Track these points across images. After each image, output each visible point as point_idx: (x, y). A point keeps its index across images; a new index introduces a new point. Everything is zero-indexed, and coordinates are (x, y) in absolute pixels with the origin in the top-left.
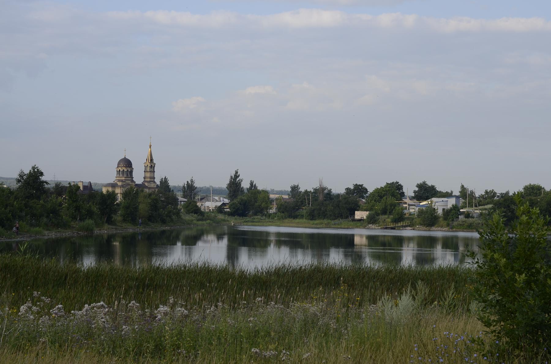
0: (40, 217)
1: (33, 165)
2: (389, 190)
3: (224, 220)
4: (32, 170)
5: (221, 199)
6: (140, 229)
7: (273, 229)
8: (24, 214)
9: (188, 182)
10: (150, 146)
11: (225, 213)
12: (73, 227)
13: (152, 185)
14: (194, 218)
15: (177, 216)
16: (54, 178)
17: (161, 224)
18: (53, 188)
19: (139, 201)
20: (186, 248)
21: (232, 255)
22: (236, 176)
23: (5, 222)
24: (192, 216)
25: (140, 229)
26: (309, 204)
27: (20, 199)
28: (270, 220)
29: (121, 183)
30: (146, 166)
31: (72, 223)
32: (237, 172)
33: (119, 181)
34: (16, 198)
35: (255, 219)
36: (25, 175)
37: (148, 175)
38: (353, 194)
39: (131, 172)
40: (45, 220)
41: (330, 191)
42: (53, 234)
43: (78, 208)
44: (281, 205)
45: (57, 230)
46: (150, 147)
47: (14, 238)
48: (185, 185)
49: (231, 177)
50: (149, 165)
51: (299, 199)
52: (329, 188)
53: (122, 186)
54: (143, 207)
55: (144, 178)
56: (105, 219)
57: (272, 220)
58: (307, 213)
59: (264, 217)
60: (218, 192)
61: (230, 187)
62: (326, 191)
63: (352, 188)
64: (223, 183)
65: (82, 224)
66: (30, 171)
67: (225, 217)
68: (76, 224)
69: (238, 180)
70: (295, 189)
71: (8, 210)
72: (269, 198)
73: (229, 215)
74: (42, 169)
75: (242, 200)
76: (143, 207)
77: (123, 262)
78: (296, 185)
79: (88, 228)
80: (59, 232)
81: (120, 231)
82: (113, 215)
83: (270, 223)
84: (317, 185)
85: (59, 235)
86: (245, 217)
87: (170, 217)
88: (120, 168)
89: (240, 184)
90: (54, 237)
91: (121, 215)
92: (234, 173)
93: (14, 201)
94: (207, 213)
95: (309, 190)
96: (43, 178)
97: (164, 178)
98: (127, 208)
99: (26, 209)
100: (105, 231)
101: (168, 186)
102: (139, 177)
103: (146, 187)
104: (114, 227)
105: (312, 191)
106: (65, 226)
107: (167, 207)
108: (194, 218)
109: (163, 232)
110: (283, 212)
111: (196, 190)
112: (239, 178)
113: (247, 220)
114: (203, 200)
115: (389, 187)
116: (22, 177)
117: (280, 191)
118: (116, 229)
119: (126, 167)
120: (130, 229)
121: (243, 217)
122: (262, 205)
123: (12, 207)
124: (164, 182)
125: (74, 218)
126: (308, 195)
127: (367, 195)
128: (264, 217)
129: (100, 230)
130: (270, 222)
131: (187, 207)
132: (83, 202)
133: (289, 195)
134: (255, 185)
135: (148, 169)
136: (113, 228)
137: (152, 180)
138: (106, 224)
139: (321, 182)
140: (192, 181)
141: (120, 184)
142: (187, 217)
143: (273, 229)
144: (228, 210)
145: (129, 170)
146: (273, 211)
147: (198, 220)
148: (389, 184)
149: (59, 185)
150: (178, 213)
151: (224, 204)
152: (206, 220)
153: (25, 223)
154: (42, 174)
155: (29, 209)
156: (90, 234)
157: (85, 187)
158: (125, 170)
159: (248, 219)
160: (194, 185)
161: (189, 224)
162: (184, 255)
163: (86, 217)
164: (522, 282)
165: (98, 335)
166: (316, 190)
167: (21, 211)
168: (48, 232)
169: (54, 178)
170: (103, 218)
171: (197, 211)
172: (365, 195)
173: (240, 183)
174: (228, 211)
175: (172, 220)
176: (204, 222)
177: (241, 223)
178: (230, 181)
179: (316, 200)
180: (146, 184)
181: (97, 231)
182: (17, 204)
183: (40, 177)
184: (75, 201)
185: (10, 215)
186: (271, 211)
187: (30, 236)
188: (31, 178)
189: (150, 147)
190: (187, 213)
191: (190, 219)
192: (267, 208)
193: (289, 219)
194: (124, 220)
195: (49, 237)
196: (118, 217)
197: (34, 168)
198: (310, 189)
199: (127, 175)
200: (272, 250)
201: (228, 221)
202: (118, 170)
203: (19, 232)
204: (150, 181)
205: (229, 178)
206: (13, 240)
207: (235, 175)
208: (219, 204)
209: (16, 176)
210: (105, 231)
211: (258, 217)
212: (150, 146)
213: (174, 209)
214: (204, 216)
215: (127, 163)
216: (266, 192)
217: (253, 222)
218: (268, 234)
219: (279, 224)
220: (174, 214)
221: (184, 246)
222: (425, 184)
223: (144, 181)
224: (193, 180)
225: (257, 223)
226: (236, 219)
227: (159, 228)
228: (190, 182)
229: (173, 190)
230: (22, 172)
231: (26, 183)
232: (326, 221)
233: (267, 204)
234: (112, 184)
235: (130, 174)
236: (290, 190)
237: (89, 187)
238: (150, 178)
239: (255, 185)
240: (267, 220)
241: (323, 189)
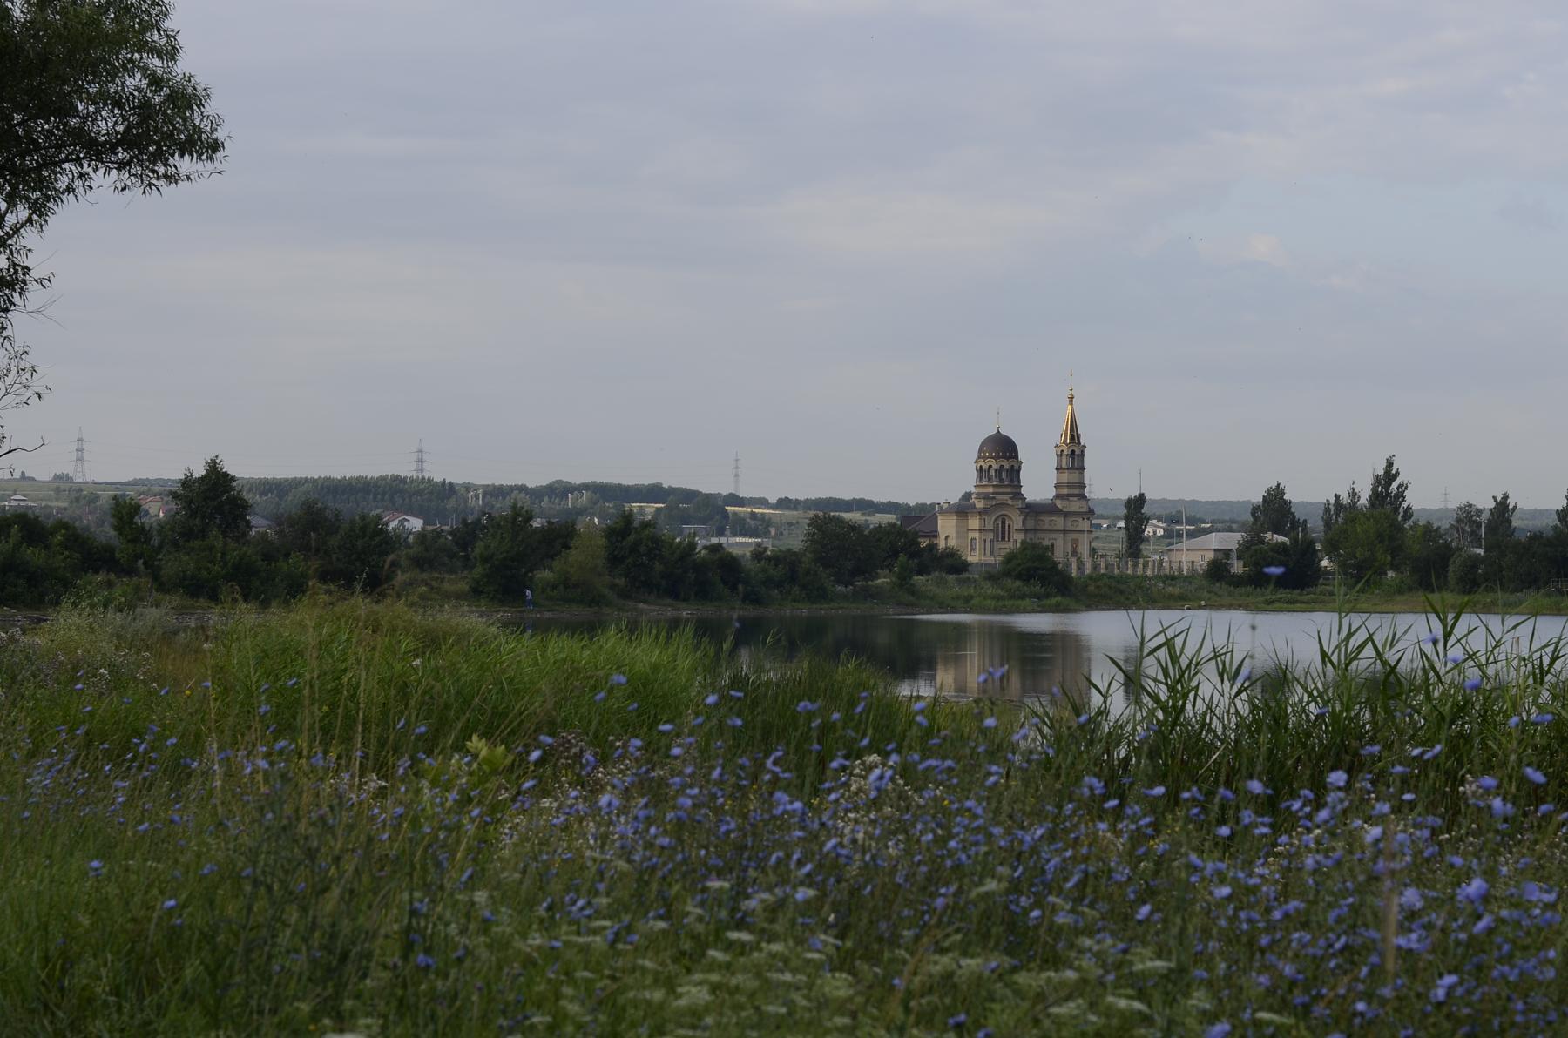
10: (1071, 399)
16: (1446, 501)
22: (1390, 475)
32: (1390, 465)
37: (1065, 477)
39: (1014, 473)
48: (1332, 507)
55: (1056, 487)
69: (1395, 485)
92: (1385, 465)
102: (1039, 483)
137: (1077, 491)
165: (331, 829)
169: (1446, 501)
180: (1059, 504)
199: (1001, 480)
215: (1002, 449)
223: (1058, 496)
232: (1500, 596)
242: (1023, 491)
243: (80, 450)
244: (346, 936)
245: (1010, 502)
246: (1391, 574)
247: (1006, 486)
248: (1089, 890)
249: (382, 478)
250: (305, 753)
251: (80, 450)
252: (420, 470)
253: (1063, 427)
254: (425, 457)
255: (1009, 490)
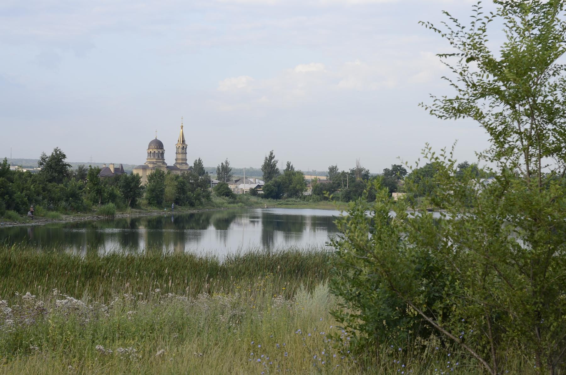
0: (59, 201)
1: (55, 148)
2: (429, 171)
3: (257, 203)
4: (54, 153)
5: (257, 180)
6: (165, 212)
7: (308, 212)
8: (41, 198)
9: (222, 163)
10: (182, 127)
11: (259, 195)
12: (94, 211)
13: (184, 167)
14: (225, 201)
15: (207, 199)
17: (189, 207)
18: (76, 171)
19: (165, 184)
20: (221, 233)
21: (267, 238)
22: (271, 157)
23: (21, 206)
24: (223, 199)
25: (165, 212)
26: (345, 186)
27: (38, 182)
28: (305, 203)
29: (152, 165)
30: (178, 147)
31: (94, 207)
32: (272, 154)
33: (150, 163)
34: (34, 181)
35: (289, 201)
36: (47, 157)
37: (180, 156)
38: (392, 175)
39: (162, 154)
40: (64, 203)
41: (367, 172)
42: (71, 219)
43: (99, 192)
44: (317, 187)
45: (76, 214)
46: (182, 128)
47: (28, 223)
48: (220, 167)
49: (266, 158)
50: (181, 147)
51: (336, 181)
52: (366, 169)
53: (153, 168)
54: (170, 190)
55: (176, 160)
56: (129, 202)
57: (307, 203)
58: (342, 194)
59: (299, 199)
60: (250, 173)
61: (265, 168)
62: (363, 172)
63: (391, 168)
64: (258, 164)
65: (103, 207)
66: (53, 153)
67: (258, 199)
68: (98, 208)
69: (273, 161)
70: (333, 170)
71: (24, 194)
72: (304, 180)
73: (262, 198)
74: (64, 152)
75: (276, 182)
76: (170, 190)
77: (150, 245)
78: (334, 165)
79: (108, 212)
80: (78, 216)
81: (144, 215)
82: (137, 199)
83: (305, 206)
84: (354, 166)
85: (77, 219)
86: (279, 199)
87: (199, 200)
88: (151, 150)
89: (275, 165)
90: (72, 221)
91: (147, 199)
92: (269, 154)
93: (31, 185)
94: (240, 195)
95: (346, 171)
96: (65, 161)
97: (198, 160)
98: (152, 191)
99: (44, 193)
100: (129, 214)
101: (202, 168)
102: (170, 159)
103: (178, 169)
104: (138, 211)
105: (349, 172)
106: (86, 210)
107: (197, 189)
108: (225, 201)
109: (192, 215)
110: (319, 195)
111: (231, 171)
112: (274, 159)
113: (281, 202)
114: (238, 183)
115: (429, 168)
116: (44, 160)
117: (322, 172)
118: (140, 212)
119: (157, 148)
120: (155, 213)
121: (277, 199)
122: (297, 187)
123: (29, 190)
124: (198, 165)
125: (95, 202)
126: (346, 177)
127: (407, 176)
128: (299, 199)
129: (123, 214)
130: (305, 204)
131: (219, 189)
132: (105, 185)
133: (327, 176)
134: (292, 166)
135: (180, 151)
136: (136, 212)
137: (184, 162)
138: (130, 208)
139: (358, 163)
140: (227, 163)
141: (151, 166)
142: (218, 200)
143: (308, 212)
144: (262, 192)
145: (161, 152)
146: (309, 192)
147: (229, 203)
148: (429, 164)
149: (83, 167)
150: (208, 196)
151: (259, 186)
152: (237, 203)
153: (41, 207)
154: (64, 156)
155: (46, 192)
156: (110, 218)
157: (116, 170)
158: (157, 152)
159: (282, 201)
160: (229, 166)
161: (219, 207)
162: (219, 238)
163: (109, 200)
164: (367, 274)
166: (353, 172)
167: (38, 195)
168: (67, 216)
170: (127, 202)
171: (228, 193)
172: (404, 176)
173: (275, 164)
174: (262, 194)
175: (201, 204)
176: (236, 205)
177: (274, 206)
178: (265, 163)
179: (353, 181)
180: (178, 166)
181: (118, 215)
182: (33, 187)
183: (63, 160)
184: (96, 184)
185: (26, 198)
186: (306, 194)
187: (46, 221)
188: (53, 161)
189: (182, 128)
190: (218, 196)
191: (221, 201)
192: (302, 190)
193: (324, 201)
194: (150, 204)
195: (66, 221)
196: (142, 200)
197: (56, 150)
198: (347, 170)
199: (159, 157)
200: (307, 232)
201: (261, 203)
202: (149, 152)
203: (34, 215)
204: (182, 163)
205: (264, 159)
206: (27, 225)
207: (270, 157)
208: (254, 186)
209: (38, 158)
210: (129, 214)
211: (293, 199)
212: (182, 127)
213: (204, 191)
214: (235, 199)
215: (159, 145)
216: (300, 173)
217: (287, 204)
218: (303, 218)
219: (314, 206)
220: (203, 197)
221: (219, 231)
222: (467, 164)
223: (176, 163)
224: (228, 161)
225: (291, 206)
226: (269, 202)
227: (186, 211)
228: (224, 164)
229: (207, 172)
230: (44, 155)
231: (48, 166)
233: (301, 186)
234: (143, 166)
235: (161, 155)
236: (328, 171)
237: (120, 170)
238: (182, 159)
239: (292, 166)
240: (302, 202)
241: (360, 170)
242: (165, 161)
245: (162, 165)
246: (71, 198)
247: (160, 159)
248: (293, 289)
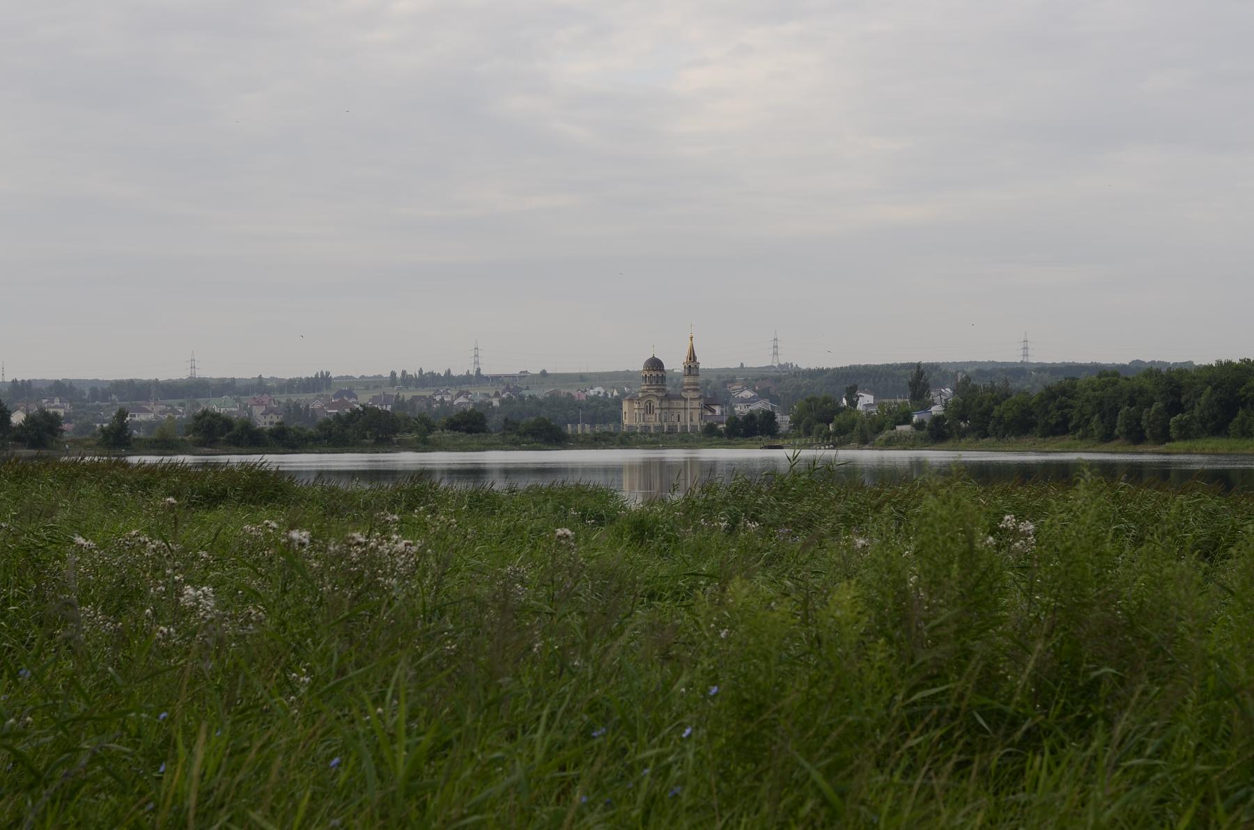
10: (691, 338)
199: (651, 382)
243: (775, 347)
244: (195, 436)
249: (842, 368)
250: (1152, 704)
251: (775, 347)
252: (1025, 355)
253: (686, 353)
254: (1029, 345)
255: (655, 387)
